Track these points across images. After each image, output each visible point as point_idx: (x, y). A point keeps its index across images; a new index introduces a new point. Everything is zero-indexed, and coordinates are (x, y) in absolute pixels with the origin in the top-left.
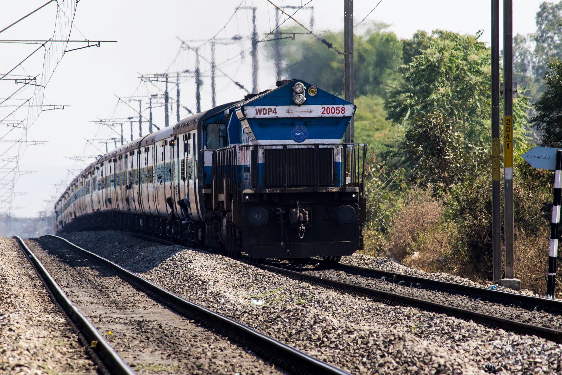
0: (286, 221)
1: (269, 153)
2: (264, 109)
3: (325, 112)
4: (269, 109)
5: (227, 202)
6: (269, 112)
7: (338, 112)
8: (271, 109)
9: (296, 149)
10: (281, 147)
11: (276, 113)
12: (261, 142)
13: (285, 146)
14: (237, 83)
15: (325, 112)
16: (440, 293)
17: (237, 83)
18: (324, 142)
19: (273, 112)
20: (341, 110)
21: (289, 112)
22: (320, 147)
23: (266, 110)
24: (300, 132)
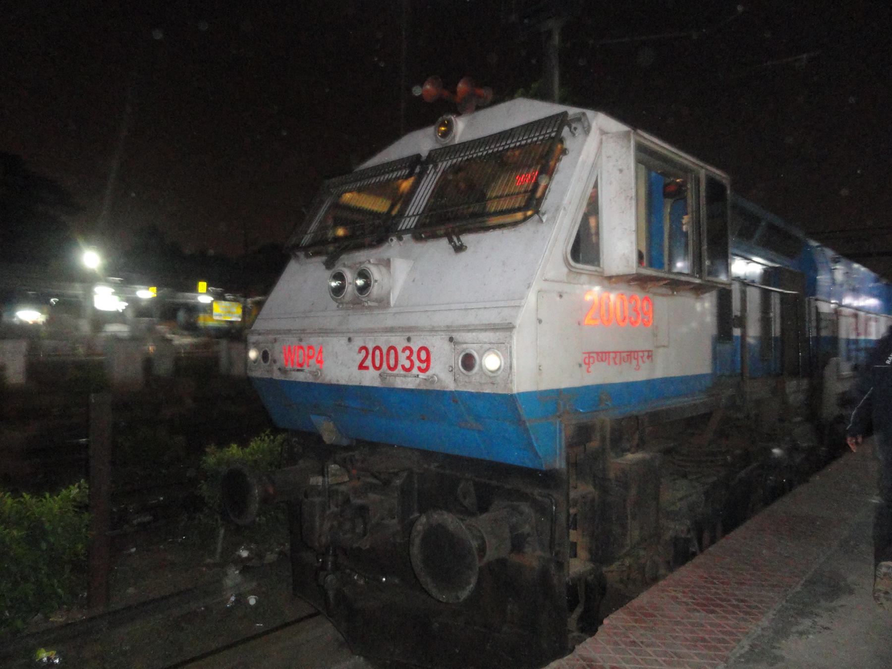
3: (368, 363)
15: (368, 363)
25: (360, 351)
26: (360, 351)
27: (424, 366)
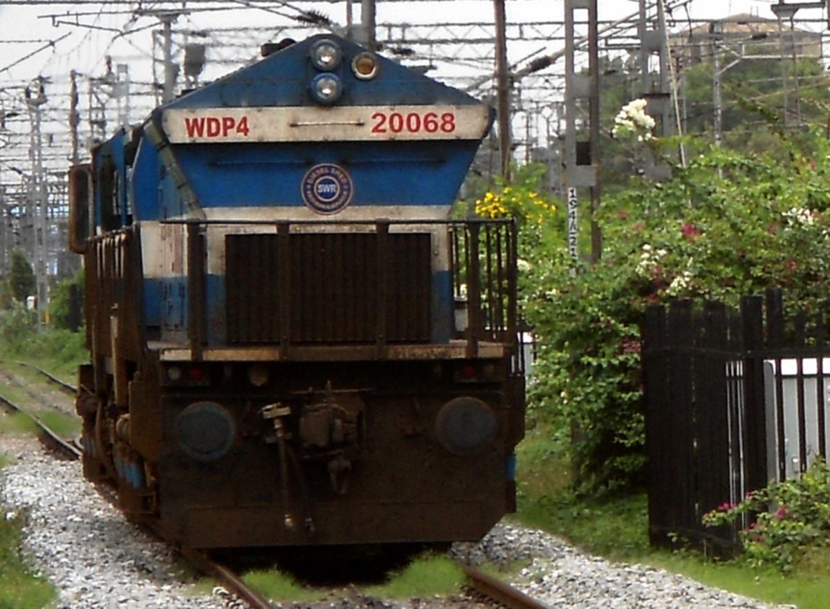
0: (289, 435)
1: (237, 244)
2: (210, 120)
3: (386, 125)
4: (225, 120)
5: (119, 377)
6: (226, 128)
7: (431, 126)
8: (232, 120)
9: (314, 235)
10: (273, 230)
11: (246, 131)
12: (215, 214)
13: (283, 226)
14: (39, 17)
16: (641, 464)
17: (39, 17)
18: (411, 217)
19: (239, 130)
20: (440, 123)
21: (294, 125)
22: (393, 229)
23: (216, 121)
24: (324, 195)
25: (374, 117)
26: (374, 117)
27: (430, 118)
